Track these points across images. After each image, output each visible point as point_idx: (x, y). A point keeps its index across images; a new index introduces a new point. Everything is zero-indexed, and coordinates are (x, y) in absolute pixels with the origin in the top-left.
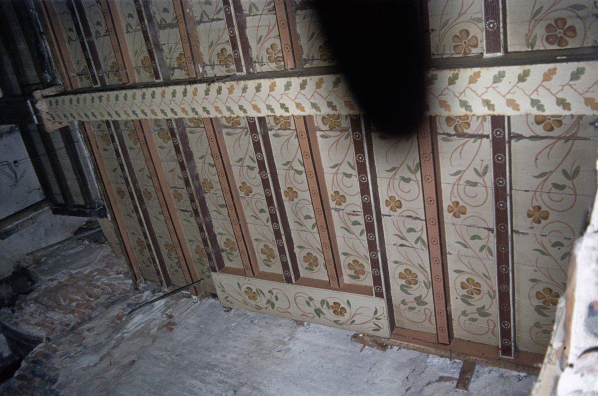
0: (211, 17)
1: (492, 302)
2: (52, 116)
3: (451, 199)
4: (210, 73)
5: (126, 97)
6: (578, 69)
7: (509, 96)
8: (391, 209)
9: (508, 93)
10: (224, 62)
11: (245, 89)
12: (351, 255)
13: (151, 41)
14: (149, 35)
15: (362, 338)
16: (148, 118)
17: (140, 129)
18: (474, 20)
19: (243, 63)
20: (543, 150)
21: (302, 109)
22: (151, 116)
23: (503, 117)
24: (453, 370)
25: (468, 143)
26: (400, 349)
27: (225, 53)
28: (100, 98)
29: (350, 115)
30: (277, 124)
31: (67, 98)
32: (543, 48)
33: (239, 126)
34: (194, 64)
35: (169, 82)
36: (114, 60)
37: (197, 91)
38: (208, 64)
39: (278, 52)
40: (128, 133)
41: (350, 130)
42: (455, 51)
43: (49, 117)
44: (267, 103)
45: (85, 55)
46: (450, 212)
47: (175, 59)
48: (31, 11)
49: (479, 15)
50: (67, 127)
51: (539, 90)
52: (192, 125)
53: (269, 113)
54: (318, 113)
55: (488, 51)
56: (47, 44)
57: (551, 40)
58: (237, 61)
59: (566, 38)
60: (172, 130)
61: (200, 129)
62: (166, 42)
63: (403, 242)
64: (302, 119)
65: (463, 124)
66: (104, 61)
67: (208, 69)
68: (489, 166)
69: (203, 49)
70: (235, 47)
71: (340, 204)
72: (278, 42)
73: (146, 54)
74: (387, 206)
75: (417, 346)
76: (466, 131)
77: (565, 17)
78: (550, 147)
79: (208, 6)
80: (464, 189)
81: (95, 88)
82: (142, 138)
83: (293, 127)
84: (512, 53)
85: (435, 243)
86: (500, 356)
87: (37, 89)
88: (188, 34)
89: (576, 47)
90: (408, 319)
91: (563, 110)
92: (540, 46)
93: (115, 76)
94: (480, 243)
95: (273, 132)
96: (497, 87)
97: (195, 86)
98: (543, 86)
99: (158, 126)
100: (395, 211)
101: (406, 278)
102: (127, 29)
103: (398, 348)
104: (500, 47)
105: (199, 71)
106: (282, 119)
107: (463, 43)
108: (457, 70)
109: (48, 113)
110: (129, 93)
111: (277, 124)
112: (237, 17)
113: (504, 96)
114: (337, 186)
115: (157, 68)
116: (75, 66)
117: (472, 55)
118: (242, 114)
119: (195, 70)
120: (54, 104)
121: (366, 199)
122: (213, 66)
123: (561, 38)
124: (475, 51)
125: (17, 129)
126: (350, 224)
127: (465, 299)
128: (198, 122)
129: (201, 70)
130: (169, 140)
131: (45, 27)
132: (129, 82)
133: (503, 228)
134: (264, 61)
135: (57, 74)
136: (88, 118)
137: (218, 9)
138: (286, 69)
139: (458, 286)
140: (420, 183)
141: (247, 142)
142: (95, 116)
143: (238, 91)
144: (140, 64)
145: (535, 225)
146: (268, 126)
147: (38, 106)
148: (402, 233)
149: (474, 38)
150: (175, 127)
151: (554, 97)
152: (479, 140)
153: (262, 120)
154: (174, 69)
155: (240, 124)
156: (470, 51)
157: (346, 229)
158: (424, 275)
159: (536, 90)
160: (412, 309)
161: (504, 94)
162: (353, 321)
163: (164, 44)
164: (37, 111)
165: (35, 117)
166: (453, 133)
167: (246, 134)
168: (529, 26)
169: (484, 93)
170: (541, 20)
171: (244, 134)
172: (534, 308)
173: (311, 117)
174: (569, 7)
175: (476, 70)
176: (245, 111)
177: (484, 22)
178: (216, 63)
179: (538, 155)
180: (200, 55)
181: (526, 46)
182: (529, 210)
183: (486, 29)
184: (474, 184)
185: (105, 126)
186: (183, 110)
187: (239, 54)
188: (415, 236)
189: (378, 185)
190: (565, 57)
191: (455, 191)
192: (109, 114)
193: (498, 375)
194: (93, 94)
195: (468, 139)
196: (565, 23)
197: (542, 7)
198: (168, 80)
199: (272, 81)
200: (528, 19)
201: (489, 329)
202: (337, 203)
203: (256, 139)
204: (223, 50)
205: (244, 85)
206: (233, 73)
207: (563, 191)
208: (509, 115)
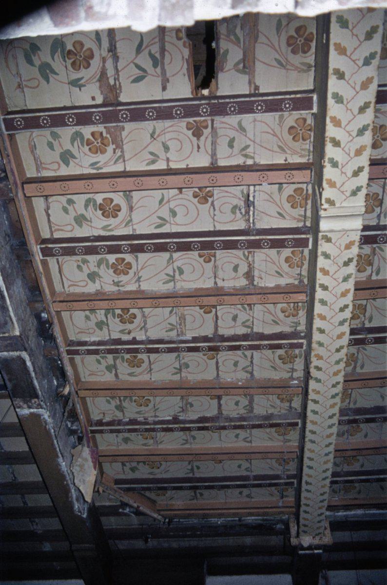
0: (249, 364)
2: (316, 535)
4: (300, 374)
5: (311, 459)
6: (337, 22)
9: (354, 89)
10: (292, 359)
11: (321, 344)
13: (262, 422)
14: (257, 423)
16: (334, 442)
17: (344, 452)
18: (280, 122)
19: (295, 341)
21: (348, 291)
22: (333, 439)
23: (379, 92)
27: (283, 357)
28: (307, 483)
29: (360, 244)
30: (359, 317)
31: (302, 515)
32: (314, 56)
33: (356, 355)
34: (289, 387)
35: (303, 415)
36: (274, 461)
37: (316, 390)
38: (291, 374)
39: (289, 307)
40: (346, 465)
41: (375, 246)
42: (308, 139)
43: (318, 538)
44: (337, 324)
45: (265, 487)
47: (282, 404)
48: (219, 523)
49: (277, 117)
50: (331, 523)
52: (347, 401)
53: (347, 324)
54: (353, 276)
55: (311, 108)
56: (248, 518)
57: (306, 49)
58: (293, 346)
60: (350, 422)
61: (353, 395)
62: (265, 409)
64: (356, 292)
65: (381, 132)
66: (274, 470)
67: (295, 375)
69: (276, 376)
70: (279, 347)
72: (279, 306)
73: (273, 430)
77: (286, 37)
78: (270, 44)
79: (235, 144)
81: (297, 485)
82: (354, 453)
83: (364, 302)
84: (315, 85)
87: (289, 541)
88: (261, 388)
89: (315, 25)
91: (378, 33)
92: (310, 58)
93: (288, 463)
95: (367, 322)
96: (347, 99)
97: (310, 390)
98: (351, 54)
99: (343, 434)
102: (248, 442)
104: (309, 97)
105: (296, 384)
106: (355, 312)
107: (301, 132)
108: (326, 139)
109: (313, 538)
110: (307, 454)
111: (359, 317)
112: (252, 340)
113: (358, 93)
115: (288, 423)
116: (274, 499)
118: (345, 351)
119: (294, 387)
120: (305, 529)
122: (293, 370)
123: (306, 39)
124: (310, 121)
125: (324, 571)
128: (346, 394)
129: (296, 382)
130: (359, 426)
131: (235, 515)
132: (297, 452)
134: (296, 321)
135: (278, 517)
136: (325, 500)
137: (242, 356)
138: (306, 302)
141: (371, 349)
142: (325, 493)
143: (321, 351)
144: (281, 438)
146: (359, 326)
147: (306, 544)
150: (347, 418)
151: (363, 44)
153: (353, 332)
154: (291, 407)
155: (354, 354)
156: (309, 125)
161: (355, 93)
163: (267, 412)
164: (310, 548)
165: (316, 551)
167: (365, 350)
168: (291, 70)
169: (352, 113)
170: (286, 59)
171: (364, 351)
173: (357, 283)
174: (278, 34)
176: (342, 347)
177: (284, 113)
178: (292, 367)
180: (281, 380)
181: (310, 72)
183: (290, 111)
185: (335, 486)
186: (332, 406)
187: (286, 344)
189: (270, 227)
190: (325, 35)
192: (324, 479)
194: (303, 489)
196: (291, 37)
197: (275, 59)
198: (300, 415)
199: (316, 317)
200: (284, 71)
203: (372, 340)
204: (280, 358)
205: (317, 344)
206: (303, 352)
208: (377, 86)
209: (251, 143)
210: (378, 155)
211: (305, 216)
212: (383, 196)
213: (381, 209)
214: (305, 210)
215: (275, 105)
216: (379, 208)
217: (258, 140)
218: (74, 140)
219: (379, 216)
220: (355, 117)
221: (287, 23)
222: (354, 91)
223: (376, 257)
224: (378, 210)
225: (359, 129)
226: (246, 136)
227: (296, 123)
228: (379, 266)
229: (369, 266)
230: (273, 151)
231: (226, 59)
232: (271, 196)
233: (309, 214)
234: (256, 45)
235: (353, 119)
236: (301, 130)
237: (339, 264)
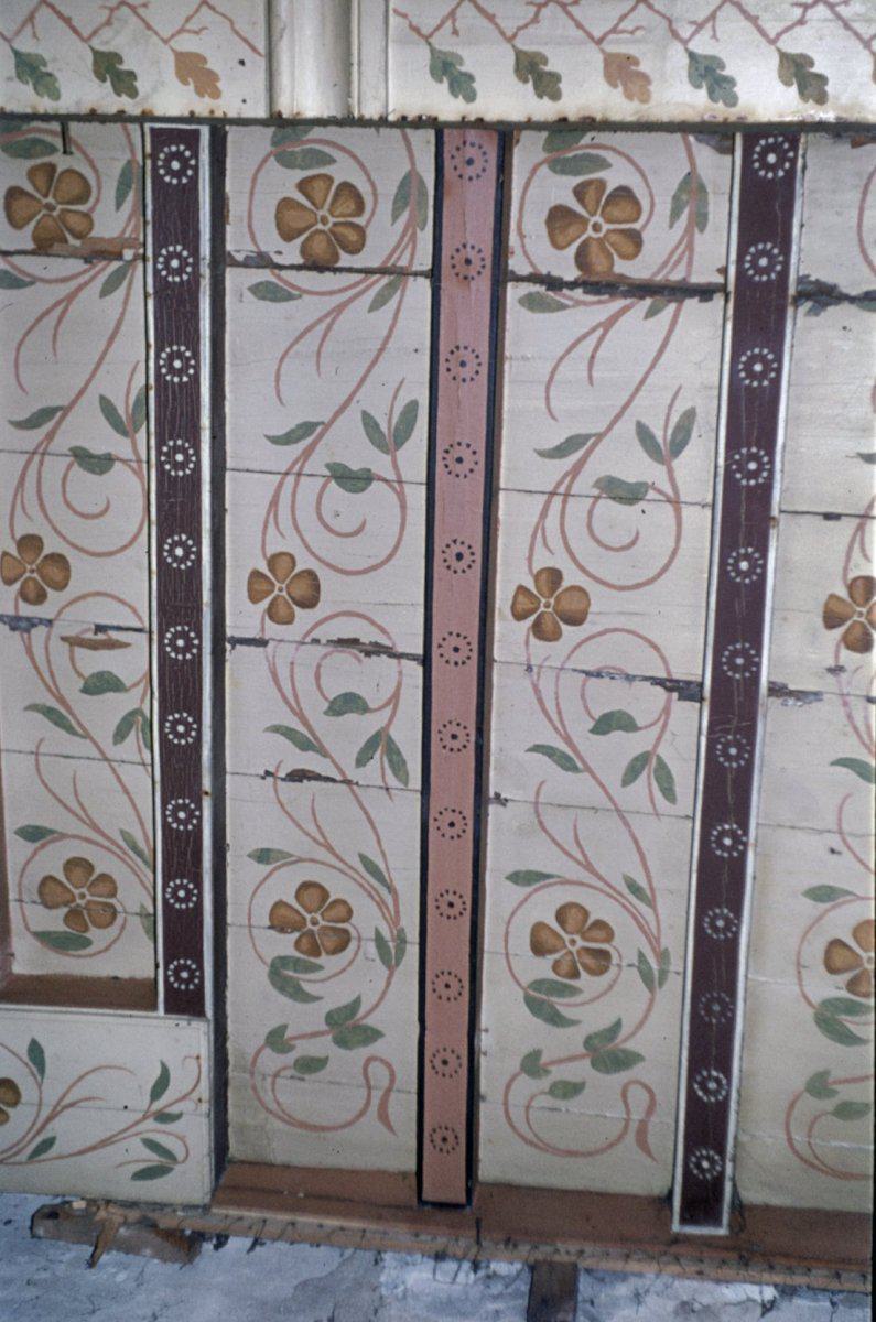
1: (652, 1001)
3: (530, 559)
8: (272, 613)
12: (63, 836)
15: (87, 1215)
24: (491, 1306)
26: (256, 1242)
46: (519, 616)
63: (311, 762)
68: (699, 419)
71: (40, 598)
74: (254, 597)
75: (332, 1222)
76: (622, 267)
80: (590, 513)
85: (456, 744)
86: (676, 1227)
90: (290, 1120)
94: (627, 746)
100: (289, 620)
101: (297, 925)
103: (248, 1242)
114: (34, 509)
121: (179, 552)
126: (71, 688)
127: (542, 1003)
133: (740, 661)
139: (521, 942)
140: (418, 496)
145: (848, 657)
148: (305, 723)
152: (672, 307)
157: (49, 712)
158: (381, 904)
160: (310, 1065)
162: (48, 1144)
166: (571, 273)
172: (810, 1012)
182: (832, 597)
184: (629, 494)
188: (362, 727)
191: (552, 522)
193: (671, 1305)
195: (628, 301)
201: (627, 1121)
202: (23, 595)
210: (522, 236)
212: (350, 270)
213: (292, 267)
216: (299, 260)
218: (558, 1014)
219: (262, 261)
220: (772, 42)
223: (77, 265)
224: (291, 253)
228: (34, 281)
229: (35, 238)
237: (106, 33)
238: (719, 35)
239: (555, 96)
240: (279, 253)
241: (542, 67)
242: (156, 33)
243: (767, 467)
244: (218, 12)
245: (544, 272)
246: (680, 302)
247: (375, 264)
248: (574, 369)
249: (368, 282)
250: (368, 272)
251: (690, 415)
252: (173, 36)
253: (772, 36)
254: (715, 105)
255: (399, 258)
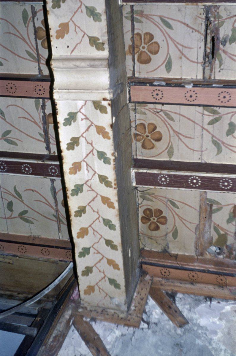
7: (90, 231)
9: (94, 230)
20: (43, 197)
25: (38, 128)
42: (138, 125)
51: (99, 255)
57: (148, 212)
59: (149, 223)
79: (227, 128)
108: (116, 187)
117: (131, 170)
123: (149, 220)
149: (152, 146)
152: (43, 140)
156: (139, 141)
159: (98, 252)
175: (116, 205)
179: (36, 191)
196: (162, 223)
197: (178, 208)
207: (7, 210)
209: (206, 126)
211: (133, 20)
212: (36, 43)
213: (34, 24)
214: (133, 29)
215: (177, 182)
217: (198, 128)
220: (88, 204)
221: (168, 235)
222: (94, 228)
225: (81, 192)
226: (213, 136)
227: (153, 144)
230: (180, 115)
231: (229, 215)
232: (182, 54)
233: (127, 25)
234: (197, 223)
235: (90, 202)
236: (147, 136)
238: (88, 192)
239: (68, 149)
240: (38, 19)
241: (75, 145)
242: (73, 16)
243: (3, 171)
244: (82, 38)
245: (46, 104)
246: (45, 142)
247: (40, 52)
248: (22, 113)
249: (34, 50)
250: (37, 49)
251: (16, 144)
252: (73, 22)
253: (90, 204)
254: (71, 191)
255: (42, 59)
